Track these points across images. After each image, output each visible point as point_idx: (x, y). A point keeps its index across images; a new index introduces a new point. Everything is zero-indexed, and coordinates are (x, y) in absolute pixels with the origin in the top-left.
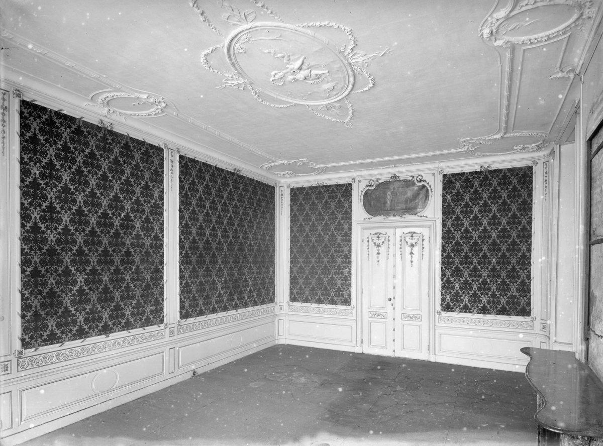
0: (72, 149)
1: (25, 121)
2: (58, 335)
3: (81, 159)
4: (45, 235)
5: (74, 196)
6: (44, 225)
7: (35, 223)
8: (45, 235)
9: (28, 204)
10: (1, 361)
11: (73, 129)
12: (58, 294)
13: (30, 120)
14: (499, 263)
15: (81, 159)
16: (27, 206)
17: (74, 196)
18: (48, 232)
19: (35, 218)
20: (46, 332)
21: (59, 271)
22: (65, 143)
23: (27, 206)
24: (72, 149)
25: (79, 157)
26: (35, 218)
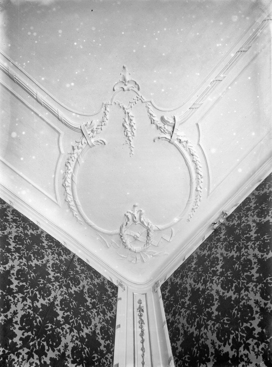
0: (102, 348)
1: (55, 328)
2: (233, 299)
3: (72, 341)
4: (10, 298)
5: (59, 330)
6: (19, 283)
7: (52, 304)
8: (10, 298)
9: (63, 317)
10: (133, 366)
11: (83, 334)
12: (233, 299)
13: (92, 312)
14: (67, 305)
15: (72, 341)
16: (62, 320)
17: (59, 330)
18: (66, 328)
19: (55, 298)
20: (254, 319)
21: (253, 276)
22: (94, 333)
23: (62, 320)
24: (102, 348)
25: (69, 337)
26: (55, 298)
